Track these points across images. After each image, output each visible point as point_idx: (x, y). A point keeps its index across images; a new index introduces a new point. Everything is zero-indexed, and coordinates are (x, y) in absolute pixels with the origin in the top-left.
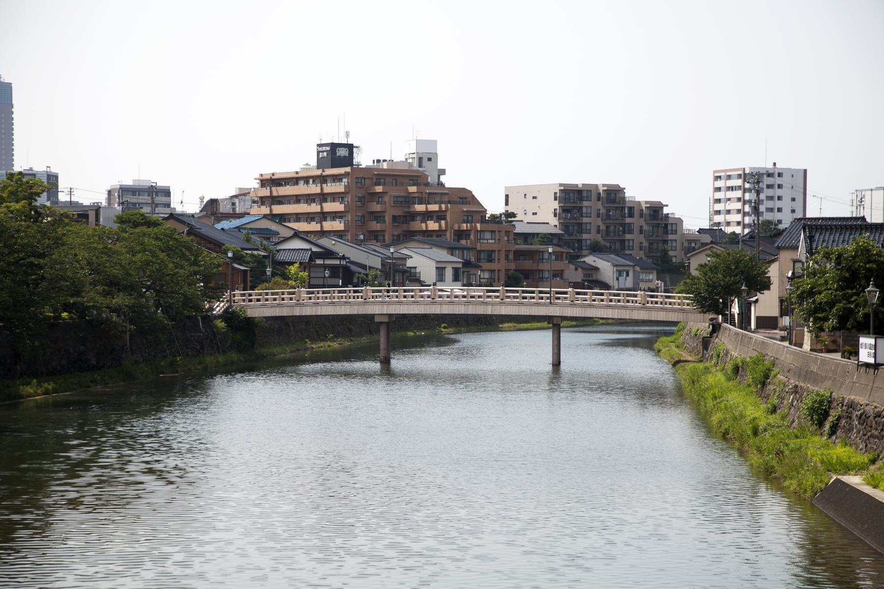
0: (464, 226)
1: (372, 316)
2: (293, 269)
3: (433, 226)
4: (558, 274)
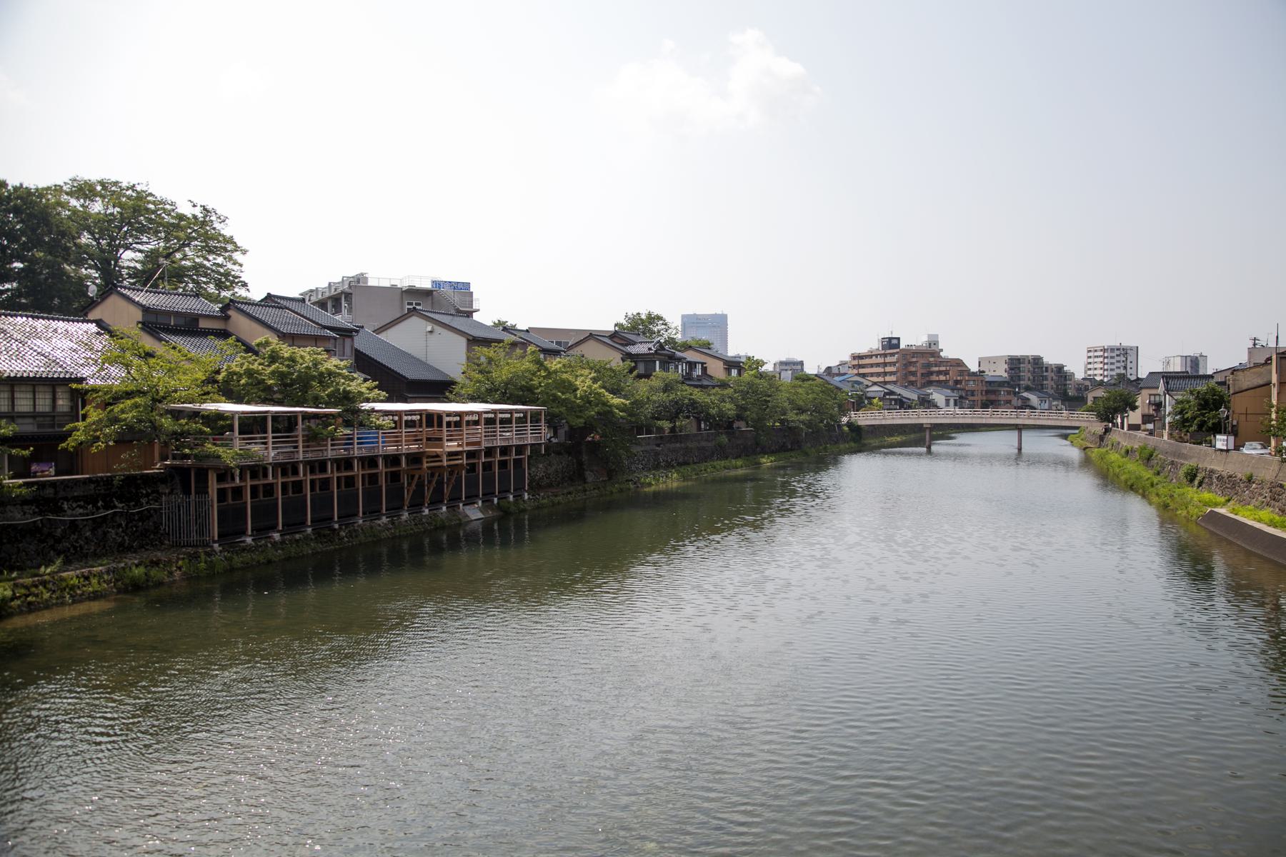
0: (959, 378)
1: (922, 424)
2: (875, 401)
3: (942, 378)
4: (1009, 402)
